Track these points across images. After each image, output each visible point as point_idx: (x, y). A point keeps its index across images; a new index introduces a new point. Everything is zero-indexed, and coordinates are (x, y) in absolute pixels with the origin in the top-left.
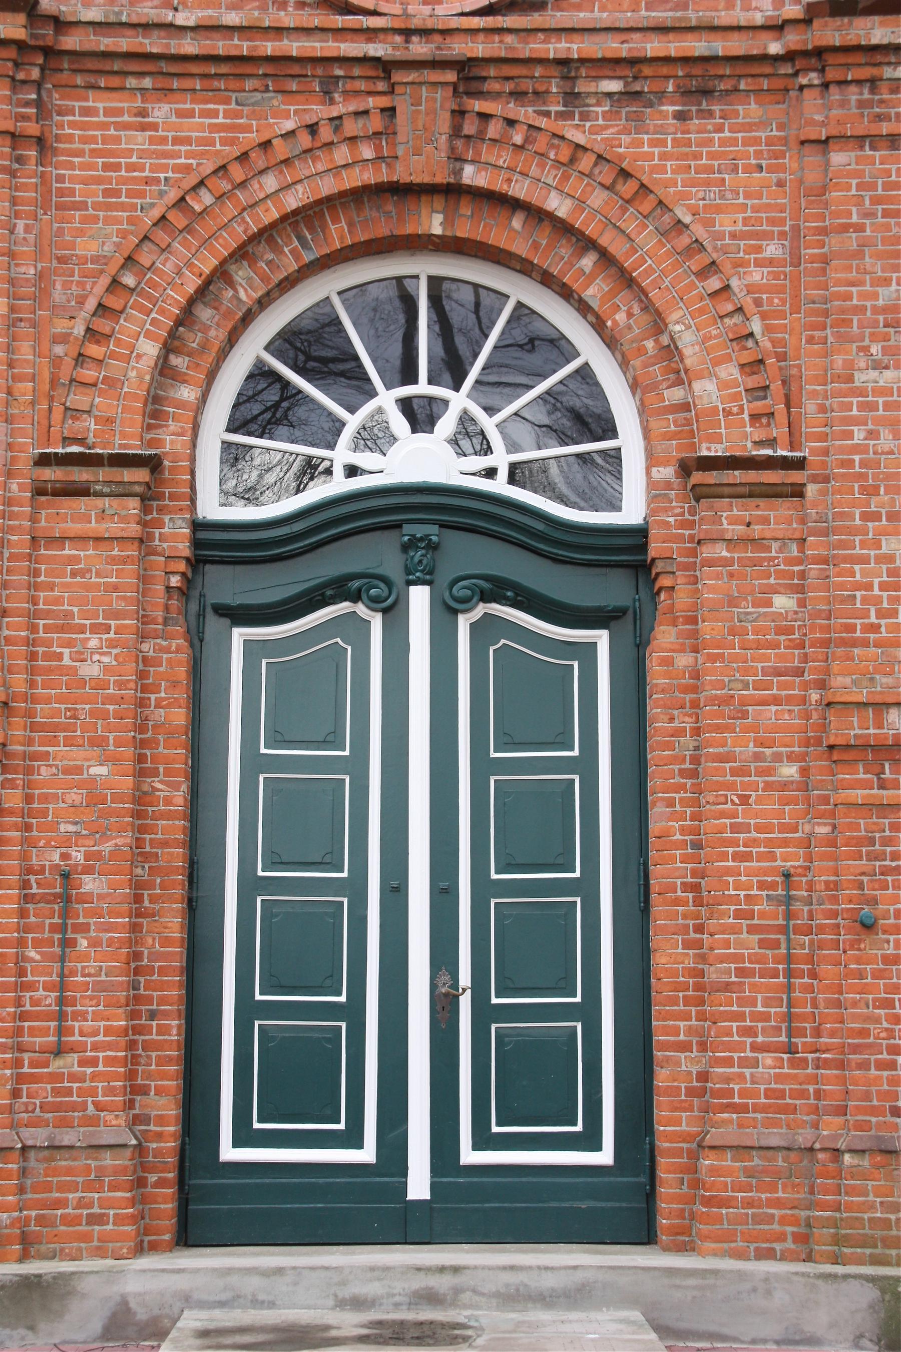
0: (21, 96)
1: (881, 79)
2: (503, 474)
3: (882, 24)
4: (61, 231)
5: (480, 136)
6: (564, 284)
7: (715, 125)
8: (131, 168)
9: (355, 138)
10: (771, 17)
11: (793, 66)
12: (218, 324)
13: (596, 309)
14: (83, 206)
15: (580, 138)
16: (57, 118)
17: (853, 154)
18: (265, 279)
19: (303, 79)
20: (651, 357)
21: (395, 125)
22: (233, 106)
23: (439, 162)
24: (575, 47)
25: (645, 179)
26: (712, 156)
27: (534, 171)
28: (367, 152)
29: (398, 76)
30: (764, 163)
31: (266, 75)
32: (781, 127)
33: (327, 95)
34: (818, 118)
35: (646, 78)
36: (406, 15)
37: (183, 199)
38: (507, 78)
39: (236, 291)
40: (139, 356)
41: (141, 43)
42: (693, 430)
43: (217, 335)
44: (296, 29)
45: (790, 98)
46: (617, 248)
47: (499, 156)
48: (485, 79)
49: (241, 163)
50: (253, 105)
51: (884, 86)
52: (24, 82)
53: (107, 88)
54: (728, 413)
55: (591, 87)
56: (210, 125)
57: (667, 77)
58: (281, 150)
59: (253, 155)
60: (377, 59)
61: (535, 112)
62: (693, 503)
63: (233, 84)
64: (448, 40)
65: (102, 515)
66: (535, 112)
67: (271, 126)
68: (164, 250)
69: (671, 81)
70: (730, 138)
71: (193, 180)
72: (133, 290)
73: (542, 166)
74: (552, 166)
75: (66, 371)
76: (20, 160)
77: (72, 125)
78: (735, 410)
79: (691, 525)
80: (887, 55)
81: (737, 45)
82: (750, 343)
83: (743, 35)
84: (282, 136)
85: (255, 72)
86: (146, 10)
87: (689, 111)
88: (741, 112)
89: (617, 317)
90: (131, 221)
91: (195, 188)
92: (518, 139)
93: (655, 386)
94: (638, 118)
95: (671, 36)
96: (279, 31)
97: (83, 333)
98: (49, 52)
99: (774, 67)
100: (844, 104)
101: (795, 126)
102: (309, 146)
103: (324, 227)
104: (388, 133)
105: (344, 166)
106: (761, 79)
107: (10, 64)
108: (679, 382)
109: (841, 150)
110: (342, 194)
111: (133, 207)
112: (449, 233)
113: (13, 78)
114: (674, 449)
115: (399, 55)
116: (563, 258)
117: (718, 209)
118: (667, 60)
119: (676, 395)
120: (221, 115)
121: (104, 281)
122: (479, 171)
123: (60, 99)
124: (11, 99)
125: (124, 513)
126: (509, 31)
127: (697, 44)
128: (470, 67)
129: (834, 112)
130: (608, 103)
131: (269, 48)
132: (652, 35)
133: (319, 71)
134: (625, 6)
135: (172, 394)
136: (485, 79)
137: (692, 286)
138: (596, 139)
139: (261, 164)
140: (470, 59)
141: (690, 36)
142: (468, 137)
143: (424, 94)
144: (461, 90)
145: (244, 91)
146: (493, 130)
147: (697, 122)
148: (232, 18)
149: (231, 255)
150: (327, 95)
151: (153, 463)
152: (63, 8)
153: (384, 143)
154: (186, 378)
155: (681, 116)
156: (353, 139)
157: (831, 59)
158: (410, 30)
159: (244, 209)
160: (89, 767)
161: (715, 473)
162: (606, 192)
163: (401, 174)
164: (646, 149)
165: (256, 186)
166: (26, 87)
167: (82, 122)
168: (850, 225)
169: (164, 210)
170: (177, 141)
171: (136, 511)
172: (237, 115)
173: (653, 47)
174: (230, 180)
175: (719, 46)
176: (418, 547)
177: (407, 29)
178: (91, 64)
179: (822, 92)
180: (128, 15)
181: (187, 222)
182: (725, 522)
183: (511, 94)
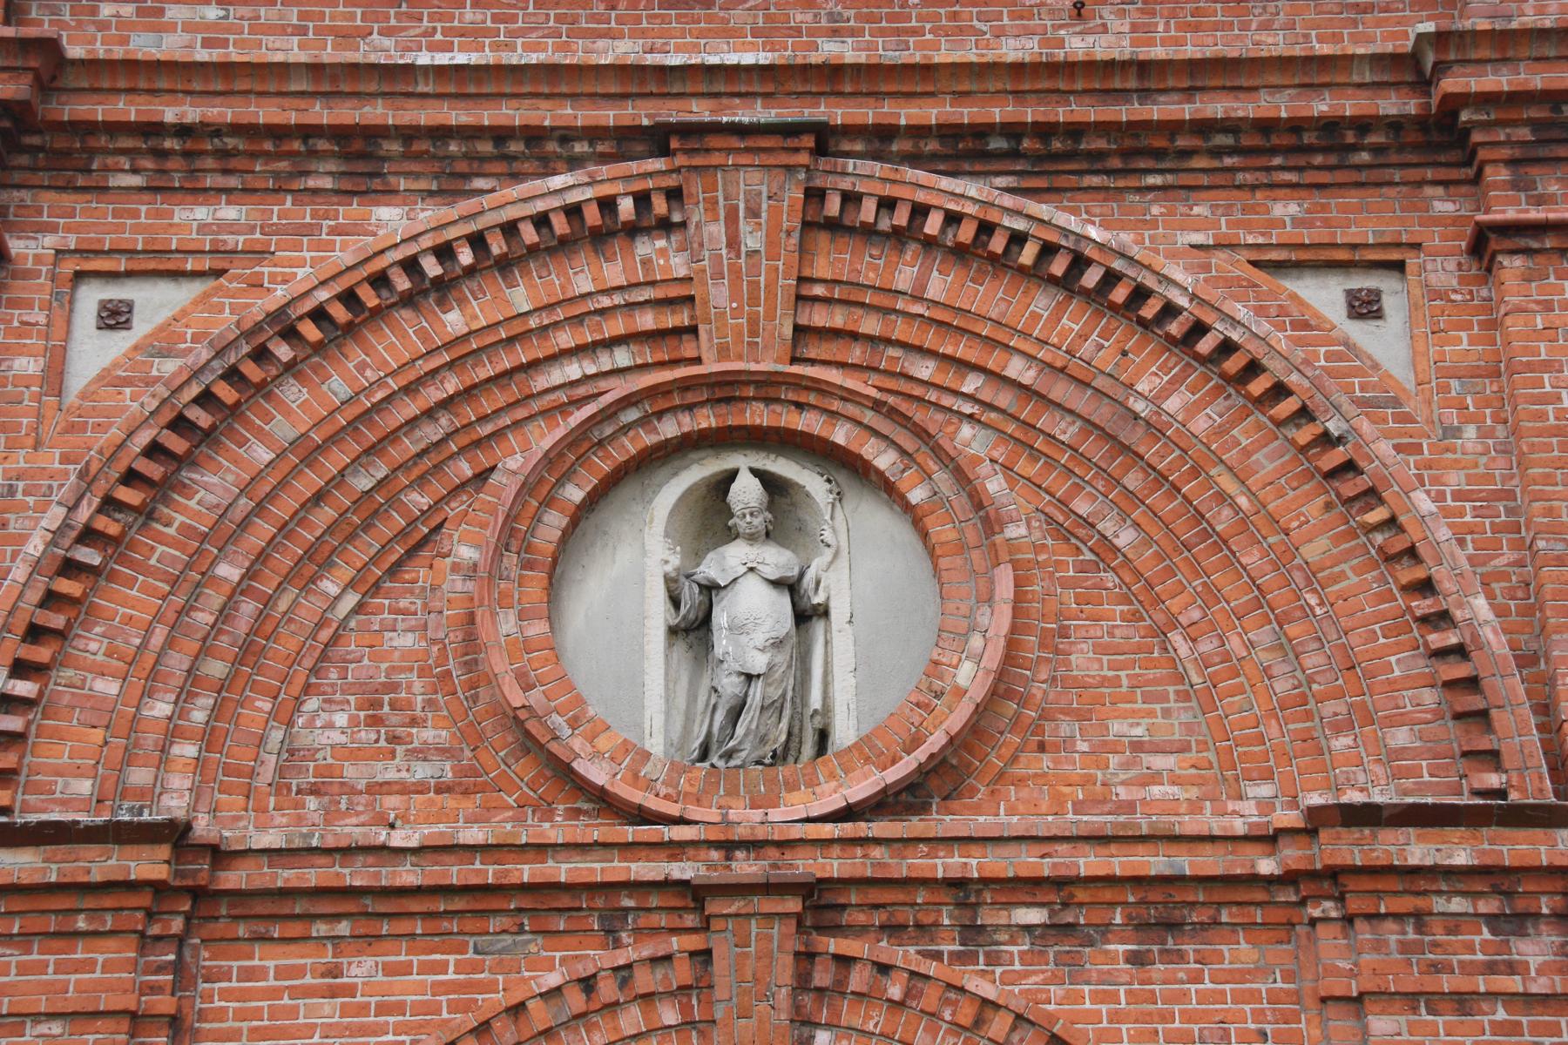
0: (152, 958)
1: (1431, 914)
3: (1420, 839)
5: (839, 989)
7: (1188, 971)
9: (652, 994)
10: (1257, 824)
11: (1297, 891)
17: (1402, 1019)
19: (575, 914)
21: (711, 975)
22: (470, 955)
23: (777, 1027)
24: (974, 862)
26: (1188, 1017)
28: (669, 1015)
29: (714, 906)
30: (1268, 1028)
31: (520, 910)
32: (1288, 976)
33: (611, 937)
34: (1344, 965)
35: (1081, 904)
36: (727, 823)
38: (876, 906)
41: (338, 874)
44: (566, 845)
45: (1298, 936)
47: (868, 1017)
48: (844, 907)
49: (478, 1037)
50: (500, 952)
51: (1436, 925)
52: (158, 938)
55: (1001, 918)
56: (434, 984)
57: (1112, 904)
59: (496, 1025)
60: (685, 883)
61: (919, 952)
63: (470, 925)
64: (788, 855)
66: (919, 952)
67: (525, 981)
69: (1119, 910)
70: (1213, 991)
74: (947, 1031)
77: (226, 995)
80: (1434, 880)
81: (1211, 862)
83: (1220, 848)
84: (541, 995)
85: (505, 906)
86: (347, 830)
87: (1149, 951)
88: (1227, 955)
92: (895, 992)
94: (1071, 962)
95: (1113, 848)
96: (541, 849)
98: (199, 894)
99: (1269, 891)
100: (1379, 946)
101: (1310, 977)
104: (701, 986)
105: (634, 1036)
106: (1252, 908)
107: (140, 915)
109: (1382, 1013)
113: (142, 934)
115: (716, 877)
118: (1110, 880)
120: (451, 968)
123: (210, 959)
124: (136, 963)
126: (878, 841)
127: (1152, 859)
128: (820, 891)
129: (1366, 957)
130: (1027, 940)
131: (526, 872)
132: (1087, 848)
133: (600, 902)
134: (1044, 808)
136: (844, 907)
138: (1012, 992)
140: (821, 881)
141: (1140, 848)
143: (754, 930)
144: (808, 923)
145: (488, 933)
146: (858, 979)
147: (1162, 967)
148: (474, 835)
152: (226, 834)
153: (694, 1002)
155: (1135, 959)
156: (647, 997)
157: (1351, 883)
158: (733, 842)
160: (377, 741)
164: (1088, 1005)
166: (161, 944)
167: (242, 989)
170: (382, 1009)
172: (476, 968)
173: (1088, 862)
175: (1185, 862)
177: (727, 841)
178: (260, 908)
179: (1344, 928)
180: (322, 836)
183: (882, 927)
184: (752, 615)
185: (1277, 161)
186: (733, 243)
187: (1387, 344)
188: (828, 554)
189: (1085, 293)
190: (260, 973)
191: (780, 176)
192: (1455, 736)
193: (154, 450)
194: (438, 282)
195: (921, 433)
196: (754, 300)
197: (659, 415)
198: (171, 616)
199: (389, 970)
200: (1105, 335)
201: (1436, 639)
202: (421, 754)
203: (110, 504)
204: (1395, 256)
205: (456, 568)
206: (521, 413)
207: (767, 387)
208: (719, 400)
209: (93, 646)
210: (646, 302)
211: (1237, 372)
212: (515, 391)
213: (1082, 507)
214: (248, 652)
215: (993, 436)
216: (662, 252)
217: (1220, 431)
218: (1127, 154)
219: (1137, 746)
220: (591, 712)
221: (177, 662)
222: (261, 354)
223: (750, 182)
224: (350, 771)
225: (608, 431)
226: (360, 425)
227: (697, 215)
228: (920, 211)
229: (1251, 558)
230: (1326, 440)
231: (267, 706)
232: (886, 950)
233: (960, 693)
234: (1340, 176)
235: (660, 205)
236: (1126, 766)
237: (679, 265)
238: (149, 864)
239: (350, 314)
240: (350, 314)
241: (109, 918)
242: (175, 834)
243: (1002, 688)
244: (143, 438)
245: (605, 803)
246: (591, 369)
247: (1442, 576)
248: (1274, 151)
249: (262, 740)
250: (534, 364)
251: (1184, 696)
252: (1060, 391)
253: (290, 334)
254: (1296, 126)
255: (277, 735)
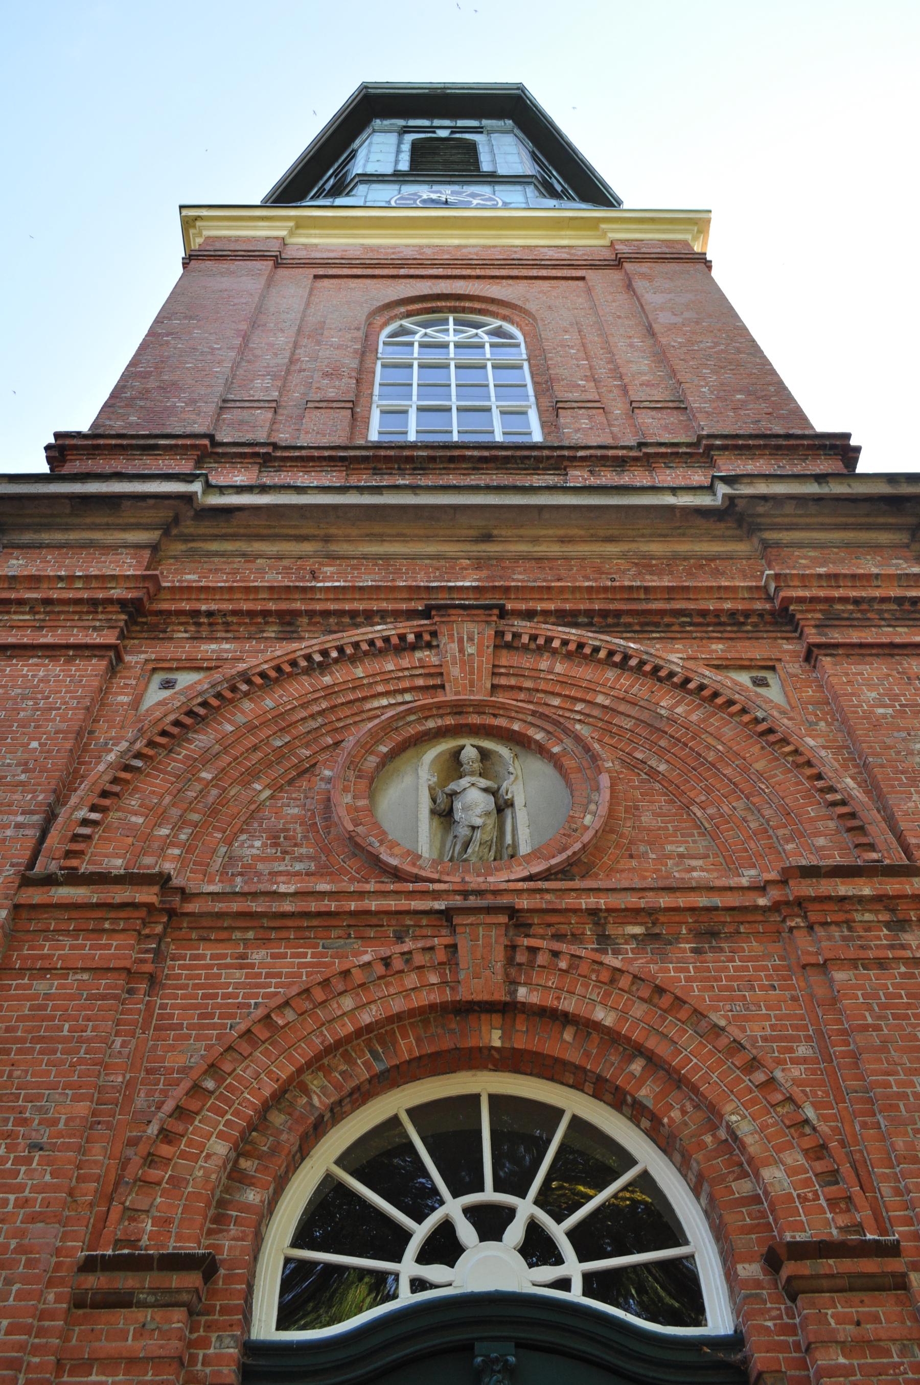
2: (577, 1285)
4: (154, 1048)
6: (617, 1088)
8: (226, 996)
9: (423, 967)
12: (290, 1129)
13: (651, 1107)
14: (180, 1026)
15: (616, 963)
16: (169, 963)
18: (338, 1087)
20: (711, 1151)
22: (320, 949)
25: (678, 992)
27: (579, 989)
28: (434, 979)
30: (776, 984)
31: (349, 926)
32: (782, 958)
35: (663, 923)
36: (463, 881)
37: (268, 1016)
38: (549, 925)
39: (310, 1098)
40: (208, 1156)
42: (769, 1224)
43: (289, 1139)
46: (663, 1050)
47: (548, 979)
48: (530, 925)
52: (148, 936)
53: (216, 940)
54: (803, 1199)
58: (358, 976)
62: (789, 1303)
65: (142, 1331)
68: (246, 1058)
71: (279, 1000)
72: (212, 1093)
73: (586, 986)
75: (134, 1170)
76: (130, 991)
77: (181, 967)
78: (810, 1195)
79: (791, 1330)
80: (853, 904)
82: (808, 1130)
89: (672, 1115)
90: (219, 1037)
91: (279, 1007)
92: (563, 965)
93: (722, 1179)
96: (362, 895)
97: (156, 1132)
98: (172, 913)
100: (830, 938)
102: (384, 973)
103: (395, 1042)
108: (744, 1175)
110: (411, 1013)
111: (224, 1026)
112: (507, 1045)
114: (753, 1242)
116: (613, 1064)
117: (746, 1019)
119: (744, 1187)
121: (186, 1085)
122: (531, 991)
125: (166, 1327)
126: (547, 891)
132: (663, 894)
135: (237, 1197)
136: (530, 925)
137: (739, 1080)
139: (340, 987)
142: (520, 965)
146: (542, 959)
149: (309, 1064)
150: (400, 939)
151: (207, 1265)
154: (254, 1181)
155: (694, 951)
157: (811, 907)
159: (323, 1024)
161: (808, 1262)
162: (645, 1005)
163: (463, 994)
165: (335, 1006)
168: (868, 1026)
169: (250, 1024)
170: (268, 975)
171: (180, 1325)
173: (664, 901)
174: (312, 1001)
176: (493, 1371)
178: (206, 922)
181: (269, 1035)
182: (832, 1322)
184: (474, 802)
185: (711, 629)
186: (462, 650)
187: (774, 693)
188: (512, 777)
189: (631, 669)
190: (202, 957)
191: (483, 625)
192: (848, 839)
193: (177, 723)
194: (320, 664)
195: (556, 723)
196: (472, 673)
197: (426, 718)
198: (175, 792)
199: (274, 956)
200: (642, 685)
201: (830, 797)
202: (300, 859)
203: (151, 744)
204: (770, 664)
205: (322, 779)
206: (357, 719)
207: (479, 707)
208: (456, 713)
209: (133, 803)
210: (421, 675)
211: (708, 696)
212: (355, 710)
213: (640, 756)
214: (213, 812)
215: (591, 728)
216: (427, 656)
217: (704, 720)
218: (642, 624)
219: (681, 856)
220: (390, 838)
221: (175, 812)
222: (234, 689)
223: (468, 628)
224: (260, 866)
225: (401, 724)
226: (280, 721)
227: (443, 640)
228: (549, 640)
229: (728, 771)
230: (757, 721)
231: (220, 836)
232: (556, 946)
233: (587, 828)
234: (739, 635)
235: (427, 637)
236: (677, 865)
237: (435, 660)
238: (148, 895)
239: (276, 677)
240: (276, 677)
241: (122, 923)
242: (162, 880)
243: (609, 827)
244: (172, 717)
245: (397, 874)
246: (393, 701)
247: (827, 771)
248: (708, 625)
249: (214, 851)
250: (365, 699)
251: (702, 834)
252: (622, 707)
253: (249, 682)
254: (717, 613)
255: (224, 850)
